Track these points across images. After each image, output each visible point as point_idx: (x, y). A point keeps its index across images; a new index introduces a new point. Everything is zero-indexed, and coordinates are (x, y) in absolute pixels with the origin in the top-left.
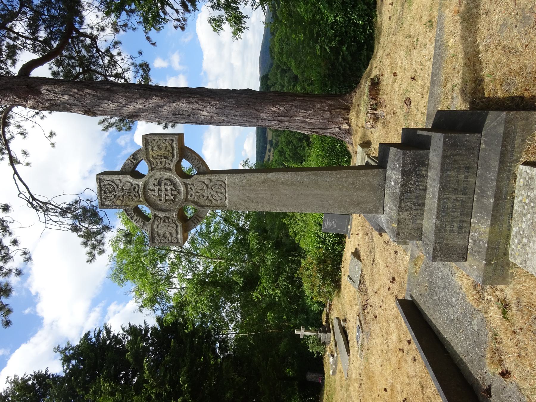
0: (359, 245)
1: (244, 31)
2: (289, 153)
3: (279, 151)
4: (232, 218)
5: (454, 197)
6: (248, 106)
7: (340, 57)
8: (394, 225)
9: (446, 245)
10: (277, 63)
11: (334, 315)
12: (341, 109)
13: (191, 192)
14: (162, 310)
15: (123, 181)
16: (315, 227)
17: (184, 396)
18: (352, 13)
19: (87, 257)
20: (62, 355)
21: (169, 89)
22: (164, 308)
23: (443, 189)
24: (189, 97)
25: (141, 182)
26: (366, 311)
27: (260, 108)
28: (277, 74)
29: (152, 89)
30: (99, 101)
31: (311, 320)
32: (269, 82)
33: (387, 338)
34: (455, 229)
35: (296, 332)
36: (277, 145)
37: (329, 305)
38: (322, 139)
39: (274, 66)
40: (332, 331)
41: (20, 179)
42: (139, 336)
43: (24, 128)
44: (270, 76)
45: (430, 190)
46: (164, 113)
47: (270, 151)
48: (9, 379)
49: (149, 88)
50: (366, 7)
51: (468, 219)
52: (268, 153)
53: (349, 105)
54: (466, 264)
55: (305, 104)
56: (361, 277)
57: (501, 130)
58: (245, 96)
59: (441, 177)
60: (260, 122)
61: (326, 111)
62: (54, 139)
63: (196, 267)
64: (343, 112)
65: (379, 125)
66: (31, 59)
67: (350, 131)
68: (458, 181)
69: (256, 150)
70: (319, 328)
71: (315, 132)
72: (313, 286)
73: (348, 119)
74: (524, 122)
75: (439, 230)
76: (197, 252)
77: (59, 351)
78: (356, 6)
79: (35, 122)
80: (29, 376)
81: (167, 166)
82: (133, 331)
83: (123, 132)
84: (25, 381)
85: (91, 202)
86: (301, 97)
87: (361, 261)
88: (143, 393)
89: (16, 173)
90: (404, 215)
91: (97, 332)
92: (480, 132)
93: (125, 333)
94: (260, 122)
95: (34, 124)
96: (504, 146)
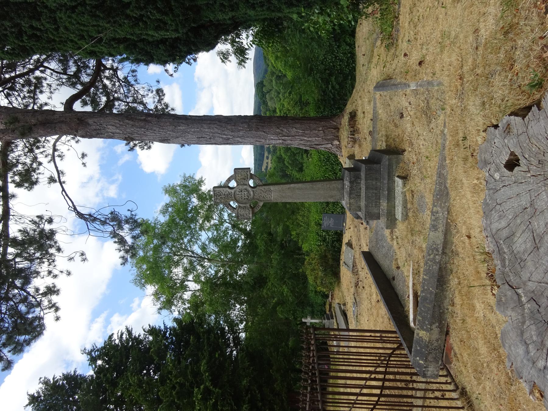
0: (351, 237)
1: (247, 61)
2: (288, 160)
3: (277, 157)
4: (239, 224)
5: (372, 191)
6: (257, 129)
7: (330, 86)
8: (348, 205)
9: (370, 212)
10: (271, 69)
11: (335, 305)
12: (332, 128)
13: (255, 194)
14: (179, 312)
15: (225, 191)
16: (316, 227)
17: (205, 384)
18: (338, 52)
19: (121, 261)
20: (89, 357)
21: (193, 117)
22: (181, 310)
23: (367, 188)
24: (210, 124)
25: (233, 191)
26: (358, 287)
27: (267, 130)
28: (272, 81)
29: (179, 118)
30: (137, 129)
31: (316, 312)
32: (264, 89)
33: (370, 299)
34: (374, 206)
35: (303, 320)
36: (274, 152)
37: (331, 295)
38: (319, 152)
39: (269, 73)
40: (334, 318)
41: (67, 195)
42: (115, 377)
43: (61, 151)
44: (264, 83)
45: (362, 189)
46: (190, 137)
47: (268, 158)
48: (41, 380)
49: (177, 117)
50: (348, 48)
51: (379, 201)
52: (265, 161)
53: (339, 126)
54: (380, 221)
55: (303, 126)
56: (353, 262)
57: (387, 163)
58: (255, 121)
59: (365, 183)
60: (267, 141)
61: (320, 131)
62: (85, 160)
63: (208, 271)
64: (334, 131)
65: (357, 146)
66: (72, 95)
67: (340, 146)
68: (373, 185)
69: (253, 157)
70: (324, 316)
71: (312, 147)
72: (316, 278)
73: (338, 137)
74: (396, 160)
75: (366, 206)
76: (208, 257)
77: (86, 353)
78: (341, 47)
79: (71, 146)
80: (58, 377)
81: (245, 183)
82: (153, 331)
83: (145, 150)
84: (55, 382)
85: (131, 212)
86: (300, 120)
87: (353, 249)
88: (168, 383)
89: (63, 190)
90: (352, 201)
91: (119, 334)
92: (380, 164)
93: (146, 334)
94: (267, 141)
95: (70, 147)
96: (389, 169)
